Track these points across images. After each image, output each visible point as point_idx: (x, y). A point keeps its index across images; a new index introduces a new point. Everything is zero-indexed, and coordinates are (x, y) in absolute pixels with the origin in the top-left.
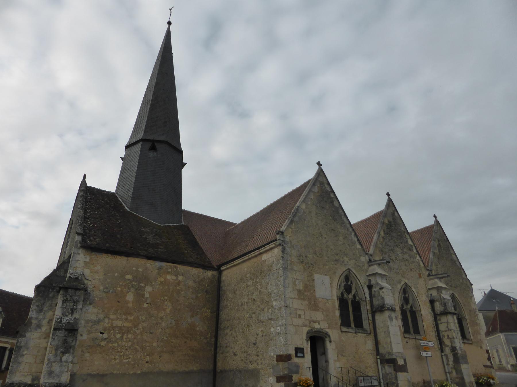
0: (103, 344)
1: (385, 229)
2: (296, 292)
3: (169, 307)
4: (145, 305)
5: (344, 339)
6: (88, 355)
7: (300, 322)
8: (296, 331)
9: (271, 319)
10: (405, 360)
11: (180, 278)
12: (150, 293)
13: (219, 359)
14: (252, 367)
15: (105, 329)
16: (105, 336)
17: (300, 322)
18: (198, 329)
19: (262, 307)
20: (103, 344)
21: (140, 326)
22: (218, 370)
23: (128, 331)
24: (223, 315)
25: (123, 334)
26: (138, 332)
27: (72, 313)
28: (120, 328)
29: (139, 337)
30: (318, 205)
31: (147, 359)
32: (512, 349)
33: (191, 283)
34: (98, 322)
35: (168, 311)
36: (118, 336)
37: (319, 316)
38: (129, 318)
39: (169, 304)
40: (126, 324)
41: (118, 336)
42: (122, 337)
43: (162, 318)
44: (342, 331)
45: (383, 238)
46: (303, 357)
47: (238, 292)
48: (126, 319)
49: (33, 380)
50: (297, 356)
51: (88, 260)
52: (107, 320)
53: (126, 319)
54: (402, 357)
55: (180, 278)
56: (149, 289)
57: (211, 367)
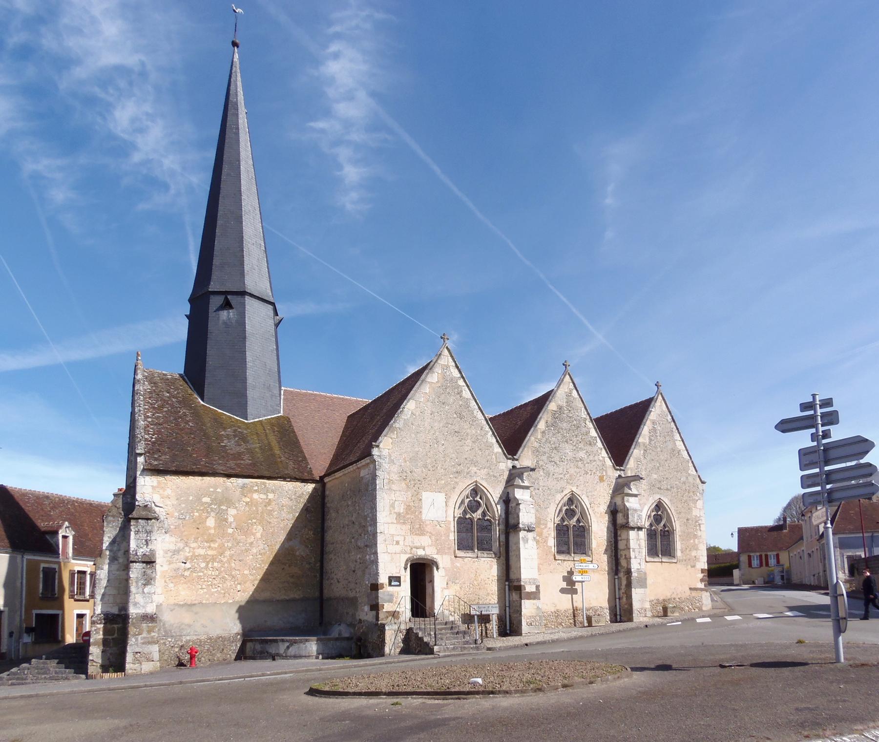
0: (187, 573)
1: (550, 420)
2: (395, 516)
3: (258, 530)
4: (230, 531)
5: (458, 565)
6: (171, 585)
7: (398, 548)
8: (392, 559)
9: (367, 546)
10: (538, 587)
11: (271, 496)
12: (234, 516)
13: (326, 583)
14: (351, 595)
15: (187, 559)
16: (188, 565)
17: (398, 548)
18: (298, 553)
19: (360, 531)
20: (187, 573)
21: (227, 553)
22: (325, 598)
23: (214, 559)
24: (328, 537)
25: (208, 563)
26: (225, 560)
27: (147, 544)
28: (204, 557)
29: (226, 565)
30: (437, 400)
31: (239, 587)
32: (846, 560)
33: (285, 501)
34: (176, 552)
35: (259, 535)
36: (203, 565)
37: (425, 541)
38: (212, 545)
39: (259, 527)
40: (210, 552)
41: (203, 565)
42: (207, 565)
43: (252, 543)
44: (456, 557)
45: (543, 432)
46: (400, 585)
47: (340, 512)
48: (209, 547)
49: (120, 610)
50: (390, 585)
51: (155, 484)
52: (187, 549)
53: (209, 547)
54: (534, 583)
55: (271, 496)
56: (232, 512)
57: (317, 594)
